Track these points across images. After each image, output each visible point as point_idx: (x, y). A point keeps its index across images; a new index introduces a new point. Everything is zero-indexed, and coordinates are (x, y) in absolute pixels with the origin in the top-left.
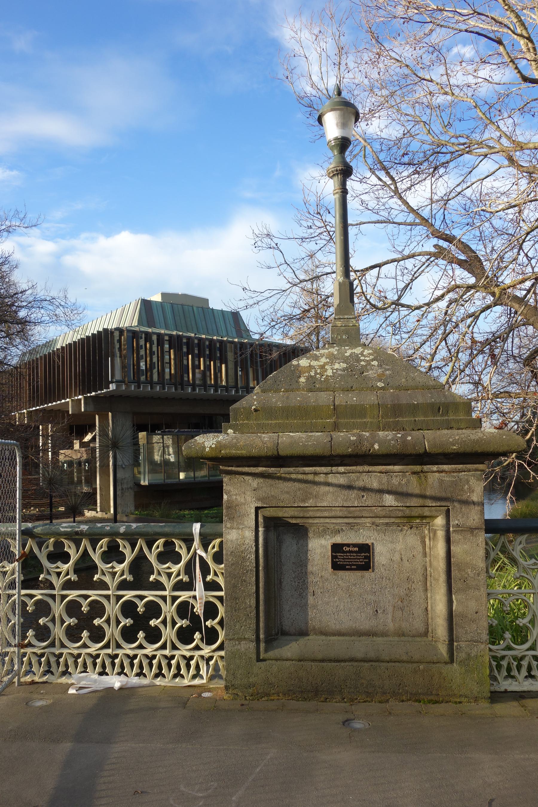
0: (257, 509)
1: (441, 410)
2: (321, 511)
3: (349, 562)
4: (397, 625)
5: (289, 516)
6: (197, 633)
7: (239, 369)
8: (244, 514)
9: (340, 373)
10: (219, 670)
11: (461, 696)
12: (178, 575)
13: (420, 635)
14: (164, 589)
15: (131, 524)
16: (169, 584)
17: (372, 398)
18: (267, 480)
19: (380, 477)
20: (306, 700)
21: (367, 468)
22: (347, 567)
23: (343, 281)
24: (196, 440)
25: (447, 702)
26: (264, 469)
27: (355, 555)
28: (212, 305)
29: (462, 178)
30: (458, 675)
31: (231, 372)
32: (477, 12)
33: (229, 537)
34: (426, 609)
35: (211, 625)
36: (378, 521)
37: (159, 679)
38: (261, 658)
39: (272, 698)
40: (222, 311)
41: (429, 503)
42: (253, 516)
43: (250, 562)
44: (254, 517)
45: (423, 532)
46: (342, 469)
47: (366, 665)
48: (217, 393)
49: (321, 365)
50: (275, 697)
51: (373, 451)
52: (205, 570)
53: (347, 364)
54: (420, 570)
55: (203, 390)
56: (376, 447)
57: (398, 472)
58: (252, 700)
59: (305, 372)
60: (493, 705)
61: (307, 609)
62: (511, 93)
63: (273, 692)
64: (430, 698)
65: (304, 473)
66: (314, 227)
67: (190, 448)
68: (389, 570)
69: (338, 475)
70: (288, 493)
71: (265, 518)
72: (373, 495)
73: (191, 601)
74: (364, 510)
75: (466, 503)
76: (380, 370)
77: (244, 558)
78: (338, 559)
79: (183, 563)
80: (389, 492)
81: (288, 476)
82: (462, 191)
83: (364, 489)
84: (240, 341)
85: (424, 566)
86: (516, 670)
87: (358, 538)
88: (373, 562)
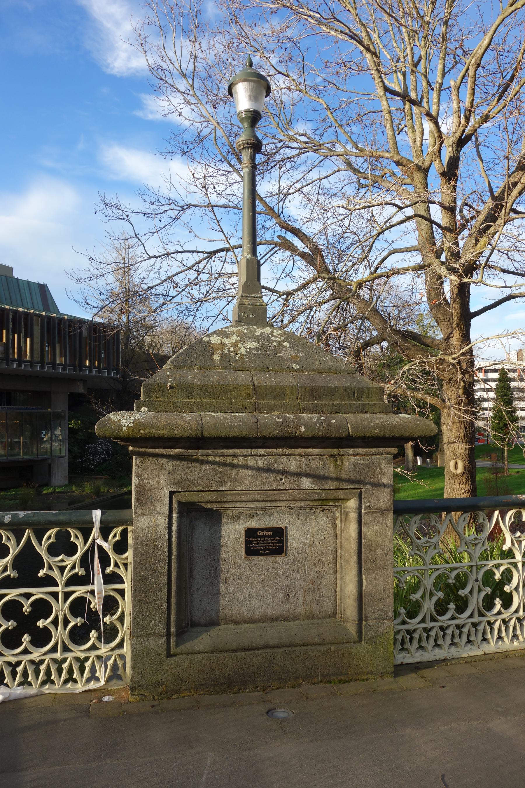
0: (171, 493)
1: (356, 395)
2: (239, 495)
3: (262, 546)
4: (307, 608)
5: (206, 501)
6: (93, 631)
7: (46, 344)
8: (157, 500)
9: (254, 352)
10: (118, 669)
11: (368, 673)
12: (73, 567)
13: (329, 617)
14: (55, 584)
15: (18, 512)
16: (61, 580)
17: (289, 380)
18: (183, 463)
19: (298, 459)
20: (218, 693)
21: (286, 451)
22: (261, 552)
23: (251, 259)
24: (110, 418)
25: (356, 680)
26: (181, 450)
27: (269, 539)
28: (17, 274)
29: (302, 175)
30: (366, 653)
31: (37, 347)
32: (336, 18)
33: (140, 525)
34: (335, 590)
35: (111, 622)
36: (293, 504)
37: (47, 686)
38: (172, 653)
39: (183, 695)
40: (28, 281)
41: (344, 485)
42: (167, 502)
43: (163, 551)
44: (168, 502)
45: (334, 514)
46: (261, 451)
47: (280, 651)
48: (20, 368)
49: (233, 343)
50: (187, 694)
51: (299, 434)
52: (105, 560)
53: (259, 343)
54: (331, 553)
55: (5, 364)
56: (302, 429)
57: (316, 455)
58: (161, 699)
59: (217, 350)
60: (396, 679)
61: (219, 598)
62: (352, 102)
63: (184, 688)
64: (340, 678)
65: (223, 456)
66: (157, 204)
67: (105, 426)
68: (301, 553)
69: (258, 458)
70: (205, 476)
71: (180, 503)
72: (291, 478)
73: (88, 596)
74: (282, 493)
75: (378, 485)
76: (293, 352)
77: (155, 547)
78: (252, 544)
79: (78, 554)
80: (307, 475)
81: (205, 458)
82: (302, 187)
83: (283, 472)
84: (48, 314)
85: (334, 547)
86: (409, 644)
87: (272, 522)
88: (287, 546)
